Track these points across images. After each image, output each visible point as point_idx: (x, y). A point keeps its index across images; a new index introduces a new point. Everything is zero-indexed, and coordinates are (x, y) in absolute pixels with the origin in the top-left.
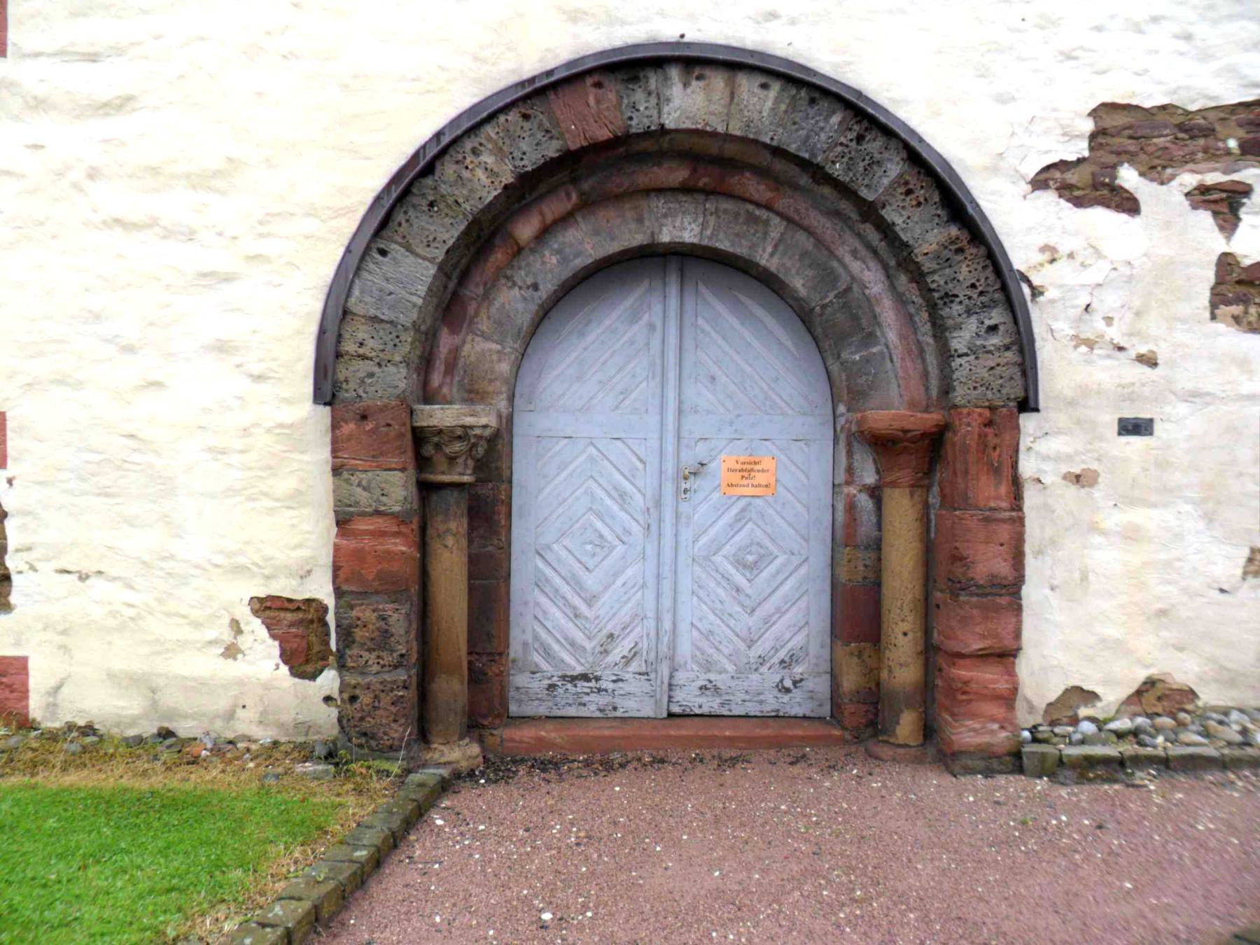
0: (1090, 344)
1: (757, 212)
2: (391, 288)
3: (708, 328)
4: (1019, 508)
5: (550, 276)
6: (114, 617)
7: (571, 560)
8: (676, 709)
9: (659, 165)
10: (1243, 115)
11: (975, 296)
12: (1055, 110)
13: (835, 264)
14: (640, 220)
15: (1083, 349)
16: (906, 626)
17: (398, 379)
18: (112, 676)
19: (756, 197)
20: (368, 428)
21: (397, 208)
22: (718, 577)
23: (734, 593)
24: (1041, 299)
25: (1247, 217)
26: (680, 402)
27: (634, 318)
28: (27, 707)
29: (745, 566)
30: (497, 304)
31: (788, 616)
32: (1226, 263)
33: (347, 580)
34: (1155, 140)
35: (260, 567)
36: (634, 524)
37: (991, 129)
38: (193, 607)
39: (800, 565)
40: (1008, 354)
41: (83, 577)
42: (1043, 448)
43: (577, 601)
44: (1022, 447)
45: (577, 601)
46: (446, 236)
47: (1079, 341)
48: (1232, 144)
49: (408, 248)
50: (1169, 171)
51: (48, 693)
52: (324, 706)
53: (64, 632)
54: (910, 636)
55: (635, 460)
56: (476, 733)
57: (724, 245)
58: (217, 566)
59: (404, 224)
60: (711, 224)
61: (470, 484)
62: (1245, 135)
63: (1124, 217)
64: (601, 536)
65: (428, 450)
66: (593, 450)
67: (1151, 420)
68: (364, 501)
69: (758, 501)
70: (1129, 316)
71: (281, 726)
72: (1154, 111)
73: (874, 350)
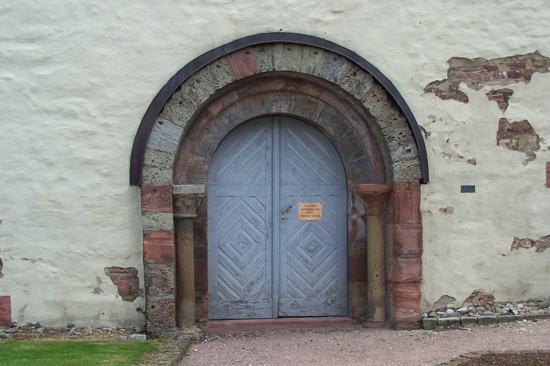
0: (450, 156)
1: (312, 99)
2: (165, 138)
3: (291, 147)
4: (421, 223)
5: (225, 128)
6: (47, 278)
7: (234, 250)
8: (281, 314)
9: (272, 82)
10: (509, 62)
11: (401, 138)
12: (434, 60)
13: (346, 121)
14: (263, 104)
15: (447, 158)
16: (376, 273)
17: (167, 176)
18: (46, 302)
19: (312, 94)
20: (156, 195)
21: (166, 105)
22: (298, 256)
23: (305, 263)
24: (429, 137)
25: (511, 104)
26: (280, 180)
27: (259, 143)
28: (10, 317)
29: (309, 251)
30: (202, 140)
31: (328, 272)
32: (503, 121)
33: (149, 258)
34: (474, 72)
35: (108, 255)
36: (261, 234)
37: (409, 67)
38: (80, 272)
39: (334, 250)
40: (414, 161)
41: (33, 261)
42: (431, 198)
43: (237, 268)
44: (422, 198)
45: (237, 268)
46: (187, 116)
47: (444, 154)
48: (505, 74)
49: (171, 121)
50: (480, 85)
51: (20, 311)
52: (137, 312)
53: (26, 285)
54: (379, 277)
55: (260, 205)
56: (198, 324)
57: (299, 114)
58: (90, 255)
59: (169, 111)
60: (293, 105)
61: (194, 218)
62: (509, 70)
63: (462, 103)
64: (247, 239)
65: (179, 204)
66: (243, 202)
67: (474, 186)
68: (155, 226)
69: (315, 223)
70: (465, 144)
71: (118, 321)
72: (474, 60)
73: (363, 157)
